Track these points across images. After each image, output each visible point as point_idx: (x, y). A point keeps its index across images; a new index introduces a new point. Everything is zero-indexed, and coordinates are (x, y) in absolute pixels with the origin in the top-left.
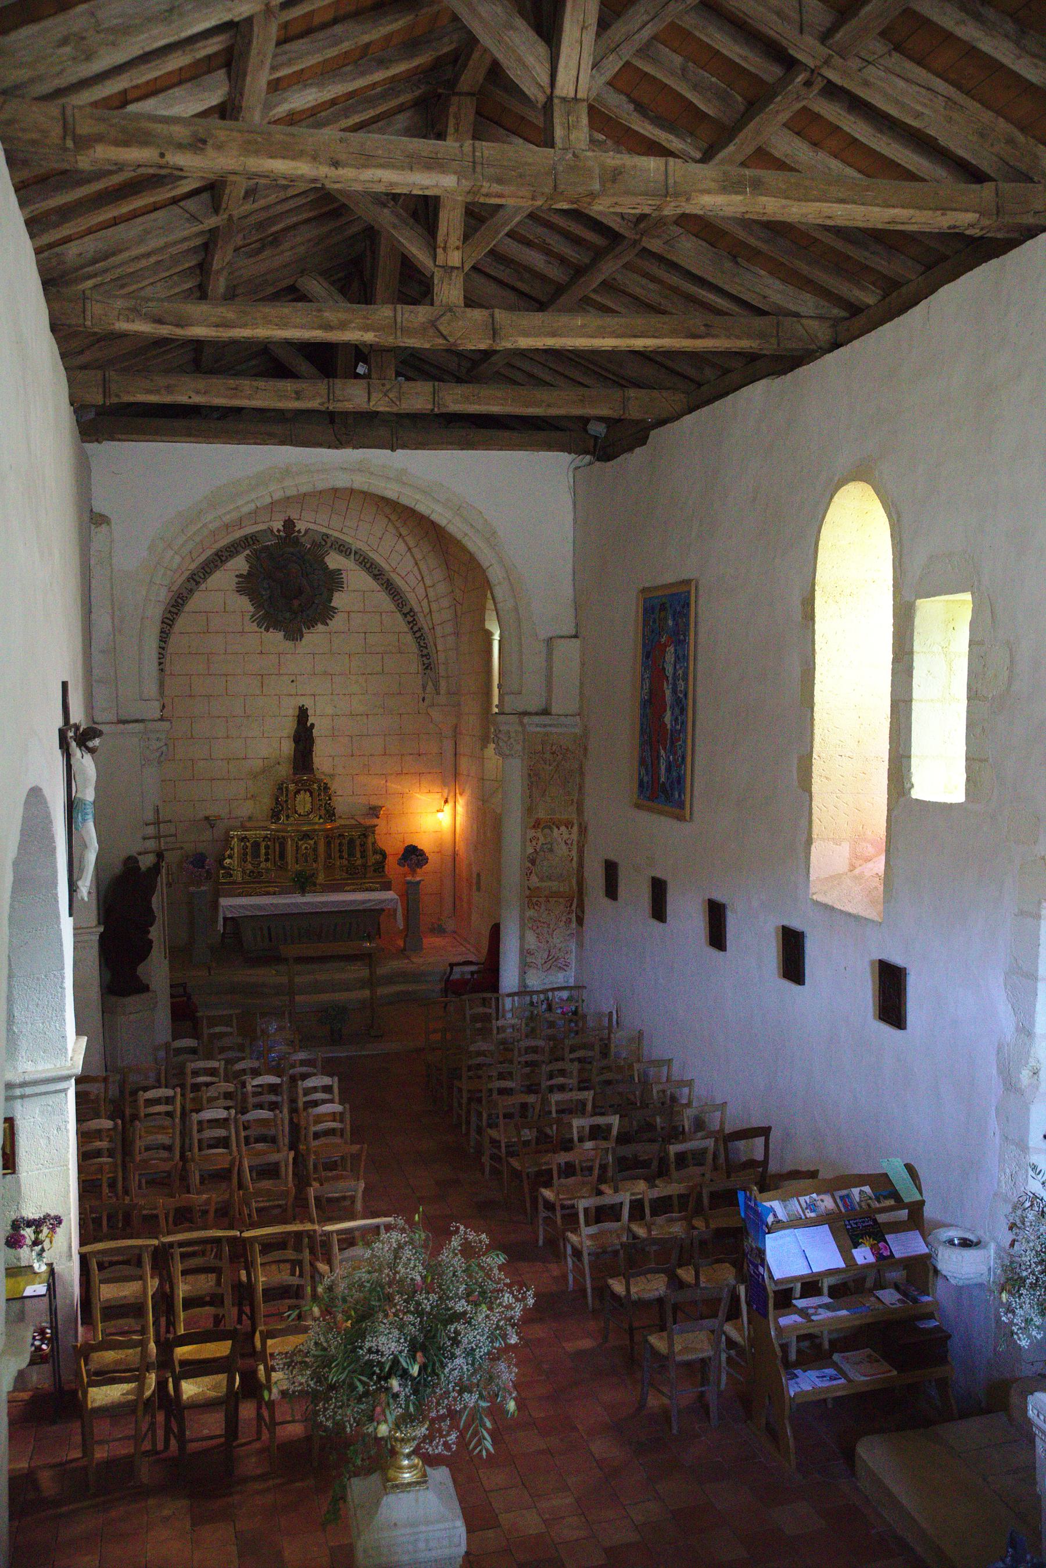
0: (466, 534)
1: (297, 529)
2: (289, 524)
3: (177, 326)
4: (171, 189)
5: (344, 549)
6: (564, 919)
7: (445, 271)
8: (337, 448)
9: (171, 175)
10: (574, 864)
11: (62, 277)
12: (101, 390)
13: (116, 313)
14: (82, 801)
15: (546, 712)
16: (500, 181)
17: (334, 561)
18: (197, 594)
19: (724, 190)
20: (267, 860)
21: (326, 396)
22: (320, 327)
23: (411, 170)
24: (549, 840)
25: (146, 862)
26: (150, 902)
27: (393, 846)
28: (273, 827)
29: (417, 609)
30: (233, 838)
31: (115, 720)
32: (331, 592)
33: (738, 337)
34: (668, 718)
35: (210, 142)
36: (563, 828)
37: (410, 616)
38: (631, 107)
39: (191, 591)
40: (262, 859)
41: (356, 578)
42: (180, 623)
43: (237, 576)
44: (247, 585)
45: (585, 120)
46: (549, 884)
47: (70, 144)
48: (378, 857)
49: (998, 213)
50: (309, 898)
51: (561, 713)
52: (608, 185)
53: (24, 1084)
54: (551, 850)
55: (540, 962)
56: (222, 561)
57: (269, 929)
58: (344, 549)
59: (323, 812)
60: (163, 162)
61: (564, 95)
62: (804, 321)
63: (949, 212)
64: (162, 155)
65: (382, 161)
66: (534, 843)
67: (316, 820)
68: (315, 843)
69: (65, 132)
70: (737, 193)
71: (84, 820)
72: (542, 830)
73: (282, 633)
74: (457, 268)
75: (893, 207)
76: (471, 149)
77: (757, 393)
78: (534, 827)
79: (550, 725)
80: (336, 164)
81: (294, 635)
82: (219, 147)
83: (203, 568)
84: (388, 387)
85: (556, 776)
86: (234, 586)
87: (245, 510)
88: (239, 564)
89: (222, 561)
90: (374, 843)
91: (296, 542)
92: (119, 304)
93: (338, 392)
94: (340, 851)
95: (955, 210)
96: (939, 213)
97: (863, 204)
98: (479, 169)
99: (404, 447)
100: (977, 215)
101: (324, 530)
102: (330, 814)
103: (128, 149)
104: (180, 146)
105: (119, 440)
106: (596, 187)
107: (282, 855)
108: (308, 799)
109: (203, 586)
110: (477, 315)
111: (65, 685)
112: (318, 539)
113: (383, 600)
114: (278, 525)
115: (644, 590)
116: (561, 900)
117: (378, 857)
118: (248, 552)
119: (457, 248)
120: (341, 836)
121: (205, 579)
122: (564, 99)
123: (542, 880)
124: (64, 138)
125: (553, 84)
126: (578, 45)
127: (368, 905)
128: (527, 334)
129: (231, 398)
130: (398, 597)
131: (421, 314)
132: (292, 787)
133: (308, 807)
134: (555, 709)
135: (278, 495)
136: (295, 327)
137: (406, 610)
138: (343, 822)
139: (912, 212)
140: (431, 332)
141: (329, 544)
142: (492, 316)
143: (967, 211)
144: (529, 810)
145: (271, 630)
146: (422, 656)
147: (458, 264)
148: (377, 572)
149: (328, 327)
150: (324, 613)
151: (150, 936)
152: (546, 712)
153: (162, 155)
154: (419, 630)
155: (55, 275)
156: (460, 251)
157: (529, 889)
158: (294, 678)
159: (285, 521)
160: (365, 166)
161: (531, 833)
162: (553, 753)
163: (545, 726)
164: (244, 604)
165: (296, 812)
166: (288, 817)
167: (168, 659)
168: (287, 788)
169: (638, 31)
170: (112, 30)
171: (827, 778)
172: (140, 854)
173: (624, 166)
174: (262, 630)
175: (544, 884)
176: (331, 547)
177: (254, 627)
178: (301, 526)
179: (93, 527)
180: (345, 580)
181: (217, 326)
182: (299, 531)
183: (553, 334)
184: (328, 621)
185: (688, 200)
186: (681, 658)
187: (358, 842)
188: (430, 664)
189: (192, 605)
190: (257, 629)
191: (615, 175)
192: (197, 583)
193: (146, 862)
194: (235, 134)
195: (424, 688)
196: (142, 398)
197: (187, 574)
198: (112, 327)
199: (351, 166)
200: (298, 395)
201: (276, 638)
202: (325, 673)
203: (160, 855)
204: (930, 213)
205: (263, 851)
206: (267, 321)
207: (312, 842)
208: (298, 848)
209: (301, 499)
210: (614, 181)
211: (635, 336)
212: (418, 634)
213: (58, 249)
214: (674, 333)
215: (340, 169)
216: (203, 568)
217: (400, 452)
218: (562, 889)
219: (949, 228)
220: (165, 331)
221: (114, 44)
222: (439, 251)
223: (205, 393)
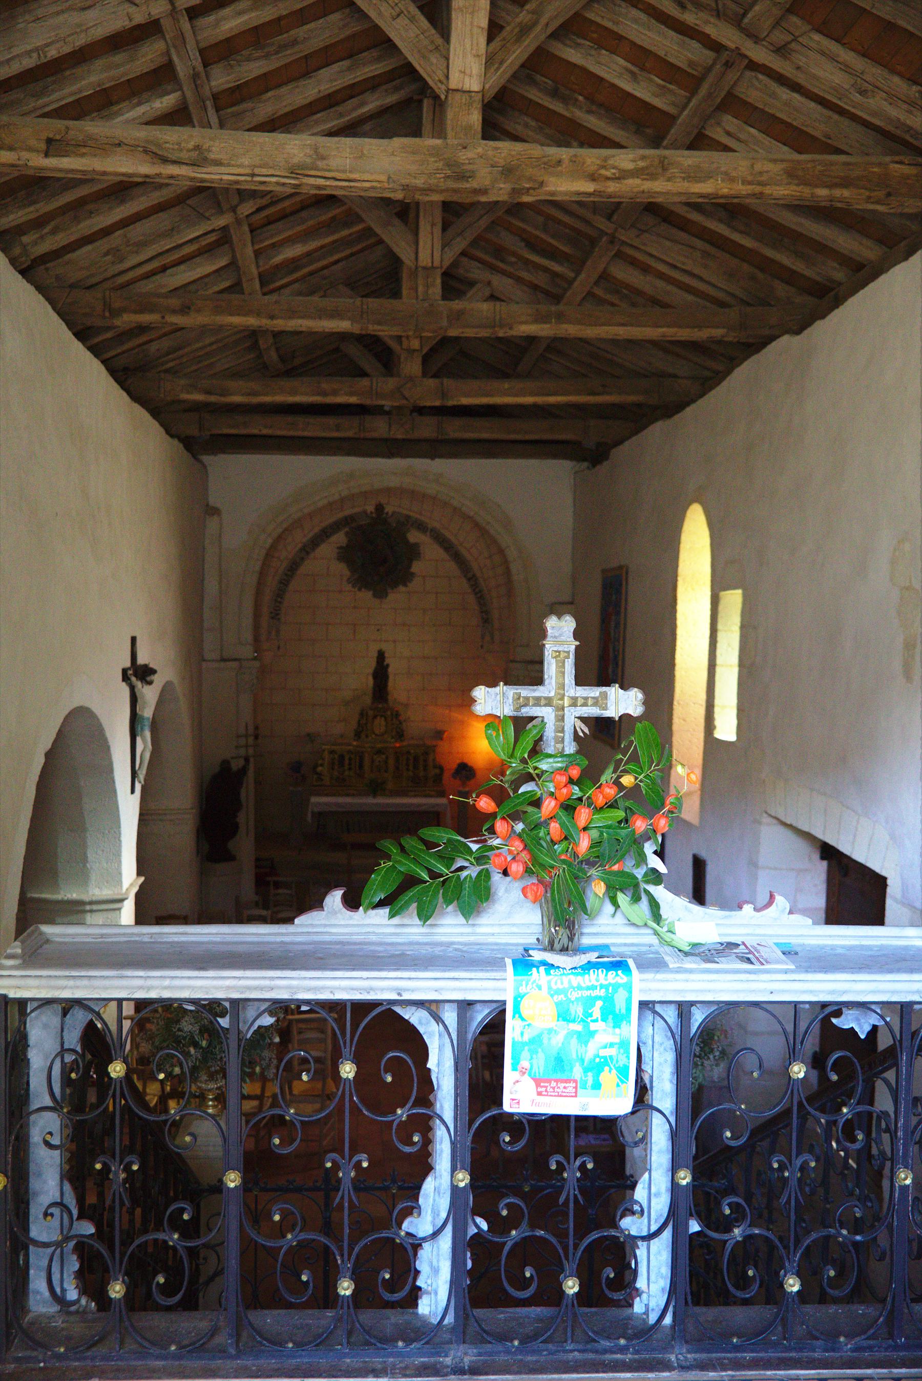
0: (489, 523)
1: (386, 511)
2: (380, 508)
3: (221, 395)
14: (142, 718)
16: (379, 323)
17: (414, 536)
18: (306, 563)
20: (350, 769)
22: (318, 394)
25: (236, 765)
26: (239, 794)
27: (451, 765)
28: (355, 743)
29: (478, 574)
30: (324, 750)
31: (219, 658)
32: (410, 561)
34: (610, 670)
38: (523, 244)
39: (302, 559)
41: (431, 551)
42: (293, 585)
44: (345, 555)
45: (438, 281)
47: (107, 314)
50: (380, 800)
53: (91, 903)
58: (421, 527)
60: (164, 321)
64: (163, 317)
67: (389, 739)
69: (104, 305)
70: (546, 323)
71: (142, 729)
73: (371, 593)
77: (657, 429)
80: (272, 317)
81: (380, 594)
82: (199, 311)
87: (321, 504)
88: (340, 538)
90: (434, 760)
92: (183, 382)
94: (407, 765)
96: (696, 330)
98: (364, 316)
99: (441, 456)
100: (725, 330)
102: (400, 735)
104: (174, 312)
106: (445, 323)
107: (361, 766)
108: (383, 722)
109: (312, 556)
110: (431, 383)
111: (134, 640)
113: (451, 566)
114: (370, 508)
115: (604, 571)
117: (437, 771)
118: (347, 529)
120: (408, 752)
121: (313, 549)
122: (424, 268)
124: (104, 311)
125: (417, 258)
126: (430, 236)
127: (423, 808)
131: (391, 383)
132: (371, 713)
133: (383, 729)
135: (345, 493)
137: (470, 575)
138: (412, 742)
139: (675, 329)
142: (442, 384)
149: (325, 394)
150: (405, 577)
153: (163, 317)
160: (290, 318)
164: (342, 569)
166: (367, 736)
169: (479, 220)
170: (135, 244)
171: (684, 720)
172: (232, 758)
177: (348, 587)
178: (389, 509)
182: (387, 513)
185: (511, 328)
186: (617, 625)
189: (304, 569)
192: (308, 553)
193: (236, 765)
194: (208, 302)
196: (226, 431)
197: (299, 546)
199: (282, 318)
200: (338, 428)
203: (247, 760)
204: (688, 330)
205: (347, 762)
207: (384, 756)
208: (373, 761)
209: (388, 491)
213: (145, 347)
216: (312, 542)
217: (438, 461)
220: (213, 399)
221: (137, 252)
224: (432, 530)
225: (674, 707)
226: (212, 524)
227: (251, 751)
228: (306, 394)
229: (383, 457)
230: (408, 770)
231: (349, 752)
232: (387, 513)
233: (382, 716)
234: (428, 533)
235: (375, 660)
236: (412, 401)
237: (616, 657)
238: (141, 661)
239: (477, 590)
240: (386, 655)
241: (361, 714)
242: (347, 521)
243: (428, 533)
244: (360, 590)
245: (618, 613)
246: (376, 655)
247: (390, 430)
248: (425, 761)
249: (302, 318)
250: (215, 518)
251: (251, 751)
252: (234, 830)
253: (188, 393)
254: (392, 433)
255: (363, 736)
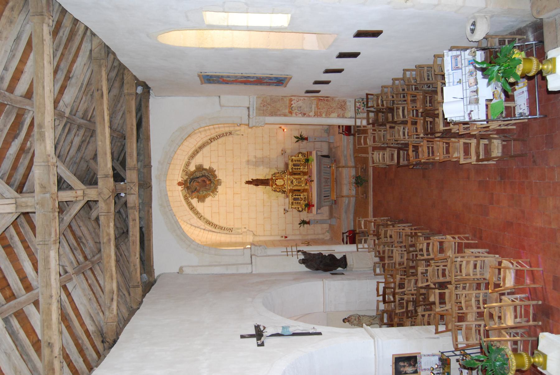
1: (181, 181)
2: (180, 184)
3: (113, 293)
4: (66, 302)
5: (188, 164)
6: (326, 102)
7: (85, 196)
8: (152, 188)
9: (62, 350)
10: (306, 98)
11: (100, 332)
12: (137, 288)
13: (110, 314)
15: (248, 108)
16: (50, 234)
17: (192, 168)
18: (205, 217)
19: (44, 140)
20: (300, 195)
21: (134, 210)
23: (50, 268)
24: (296, 108)
29: (209, 137)
33: (101, 76)
35: (49, 341)
36: (292, 103)
37: (212, 140)
40: (300, 197)
41: (198, 160)
42: (215, 222)
43: (199, 202)
44: (202, 199)
46: (313, 108)
48: (300, 155)
49: (42, 15)
51: (249, 103)
52: (47, 190)
54: (300, 107)
55: (342, 112)
56: (193, 208)
57: (324, 197)
58: (188, 164)
59: (283, 175)
61: (15, 208)
62: (93, 49)
63: (44, 38)
64: (56, 357)
65: (48, 280)
66: (297, 114)
68: (294, 179)
70: (45, 135)
72: (292, 110)
73: (219, 186)
74: (84, 191)
75: (44, 64)
76: (39, 246)
78: (291, 114)
79: (253, 107)
80: (51, 297)
83: (196, 214)
84: (129, 187)
85: (273, 105)
86: (202, 203)
88: (194, 201)
89: (193, 208)
91: (186, 181)
93: (132, 205)
95: (43, 35)
96: (44, 42)
97: (44, 78)
98: (46, 243)
99: (150, 162)
101: (181, 171)
103: (55, 369)
104: (52, 351)
105: (153, 264)
106: (48, 195)
107: (299, 190)
109: (203, 214)
110: (100, 183)
111: (242, 337)
112: (184, 173)
113: (206, 150)
114: (180, 188)
116: (319, 104)
119: (76, 192)
121: (200, 214)
122: (16, 208)
123: (311, 111)
125: (12, 213)
128: (106, 165)
129: (136, 244)
130: (205, 144)
132: (274, 186)
133: (281, 180)
134: (248, 106)
136: (110, 252)
137: (209, 141)
140: (108, 201)
141: (186, 169)
143: (43, 29)
144: (285, 115)
145: (217, 190)
146: (226, 135)
147: (82, 192)
148: (196, 152)
149: (109, 240)
150: (211, 171)
151: (327, 255)
152: (248, 108)
153: (56, 357)
154: (217, 136)
155: (100, 334)
156: (77, 191)
157: (315, 116)
158: (235, 183)
159: (179, 185)
160: (51, 285)
161: (294, 115)
162: (264, 106)
163: (253, 109)
164: (208, 200)
165: (283, 185)
166: (285, 188)
167: (228, 226)
168: (274, 188)
173: (39, 183)
174: (217, 193)
175: (313, 110)
176: (187, 169)
178: (180, 180)
179: (183, 273)
180: (199, 164)
181: (112, 279)
182: (182, 180)
183: (106, 154)
184: (214, 170)
185: (49, 156)
186: (228, 77)
187: (294, 162)
188: (229, 133)
189: (210, 219)
190: (218, 195)
191: (43, 187)
192: (201, 216)
193: (302, 257)
194: (45, 332)
195: (238, 135)
197: (198, 220)
198: (116, 315)
199: (51, 291)
201: (220, 189)
202: (233, 171)
204: (45, 47)
205: (297, 197)
206: (109, 262)
207: (294, 180)
210: (45, 188)
211: (104, 120)
212: (218, 137)
214: (102, 104)
215: (53, 295)
217: (153, 164)
218: (315, 103)
219: (50, 35)
222: (78, 199)
223: (135, 253)
224: (189, 160)
225: (271, 48)
226: (187, 271)
227: (294, 249)
228: (110, 249)
229: (152, 190)
230: (300, 169)
231: (292, 196)
232: (182, 180)
233: (275, 181)
234: (190, 161)
235: (250, 185)
236: (111, 194)
237: (245, 77)
238: (254, 332)
239: (216, 138)
240: (247, 180)
241: (275, 191)
242: (186, 198)
243: (190, 161)
244: (217, 192)
245: (222, 77)
246: (247, 185)
247: (134, 194)
248: (295, 161)
249: (50, 279)
250: (184, 269)
251: (294, 249)
252: (332, 257)
253: (113, 310)
254: (135, 193)
255: (284, 190)
